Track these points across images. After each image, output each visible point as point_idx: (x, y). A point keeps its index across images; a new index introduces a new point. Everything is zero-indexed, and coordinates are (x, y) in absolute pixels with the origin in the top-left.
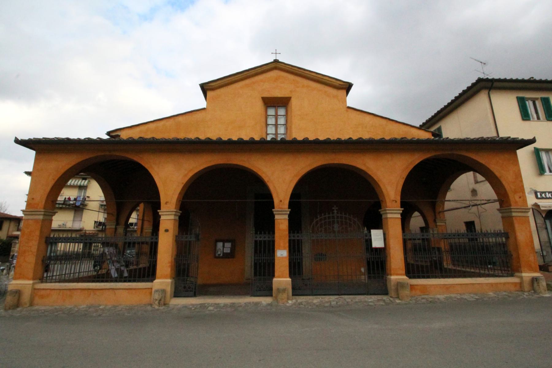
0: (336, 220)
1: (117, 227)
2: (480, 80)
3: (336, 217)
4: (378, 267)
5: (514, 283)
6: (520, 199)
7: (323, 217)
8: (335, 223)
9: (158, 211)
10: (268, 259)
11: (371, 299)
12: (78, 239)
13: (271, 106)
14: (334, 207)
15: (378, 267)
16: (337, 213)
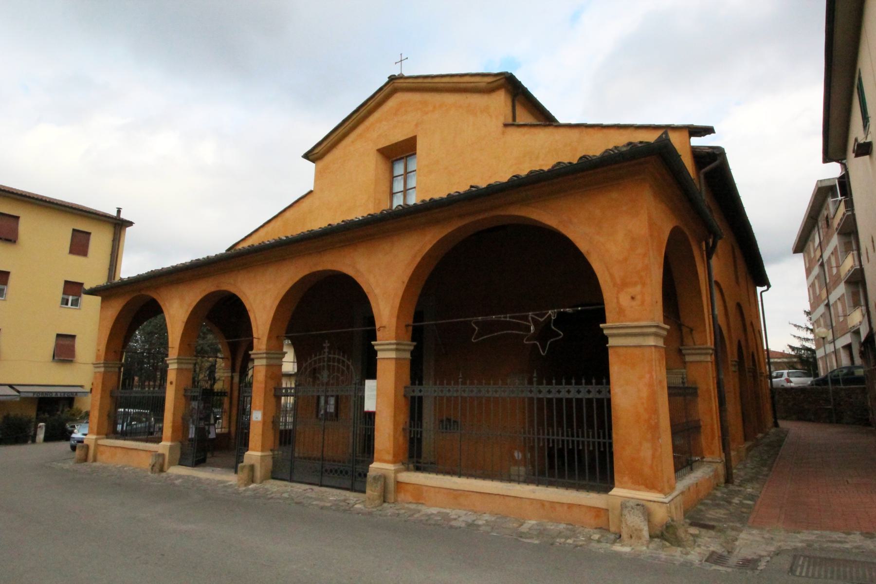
1: (233, 374)
3: (326, 359)
4: (571, 465)
5: (594, 508)
6: (634, 303)
9: (373, 343)
10: (558, 440)
11: (333, 495)
13: (397, 160)
14: (325, 343)
15: (571, 465)
16: (329, 353)
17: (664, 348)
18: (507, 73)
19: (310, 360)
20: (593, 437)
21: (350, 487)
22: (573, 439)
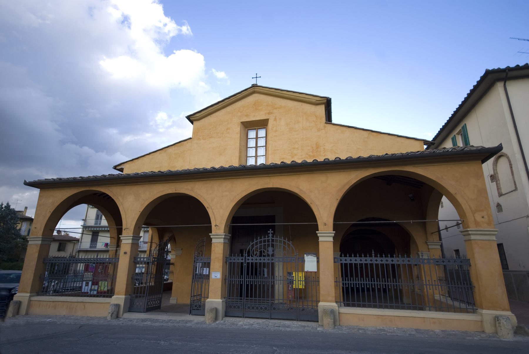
0: (270, 243)
1: (117, 248)
2: (488, 73)
3: (270, 240)
7: (259, 240)
8: (269, 247)
12: (83, 259)
14: (272, 231)
17: (228, 243)
18: (329, 97)
19: (260, 239)
20: (380, 282)
21: (270, 317)
22: (380, 283)
